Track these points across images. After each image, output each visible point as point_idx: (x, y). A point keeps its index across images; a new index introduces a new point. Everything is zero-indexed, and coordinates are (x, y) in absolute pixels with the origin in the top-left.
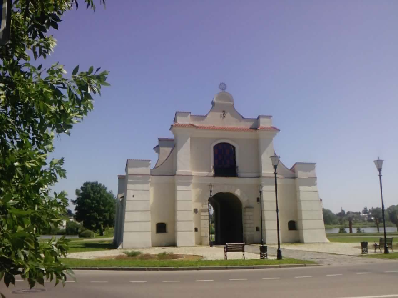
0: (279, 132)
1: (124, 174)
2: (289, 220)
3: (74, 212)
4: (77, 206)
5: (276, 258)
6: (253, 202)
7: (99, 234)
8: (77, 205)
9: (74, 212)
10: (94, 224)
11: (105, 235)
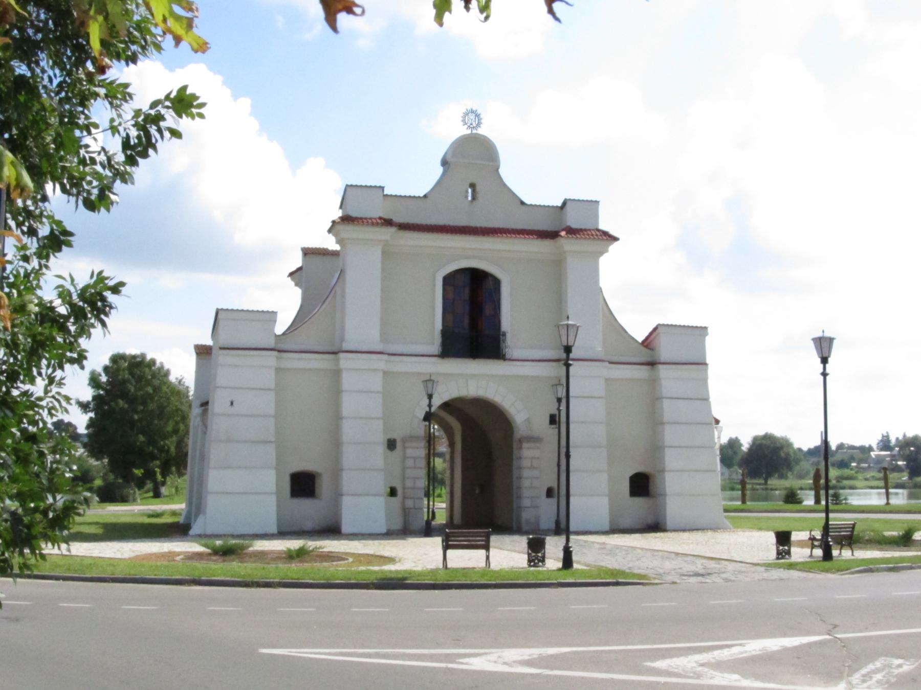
0: (616, 243)
1: (209, 342)
2: (632, 472)
3: (82, 430)
4: (91, 418)
5: (560, 565)
6: (541, 426)
7: (151, 494)
8: (92, 415)
9: (82, 430)
10: (138, 468)
11: (167, 496)
